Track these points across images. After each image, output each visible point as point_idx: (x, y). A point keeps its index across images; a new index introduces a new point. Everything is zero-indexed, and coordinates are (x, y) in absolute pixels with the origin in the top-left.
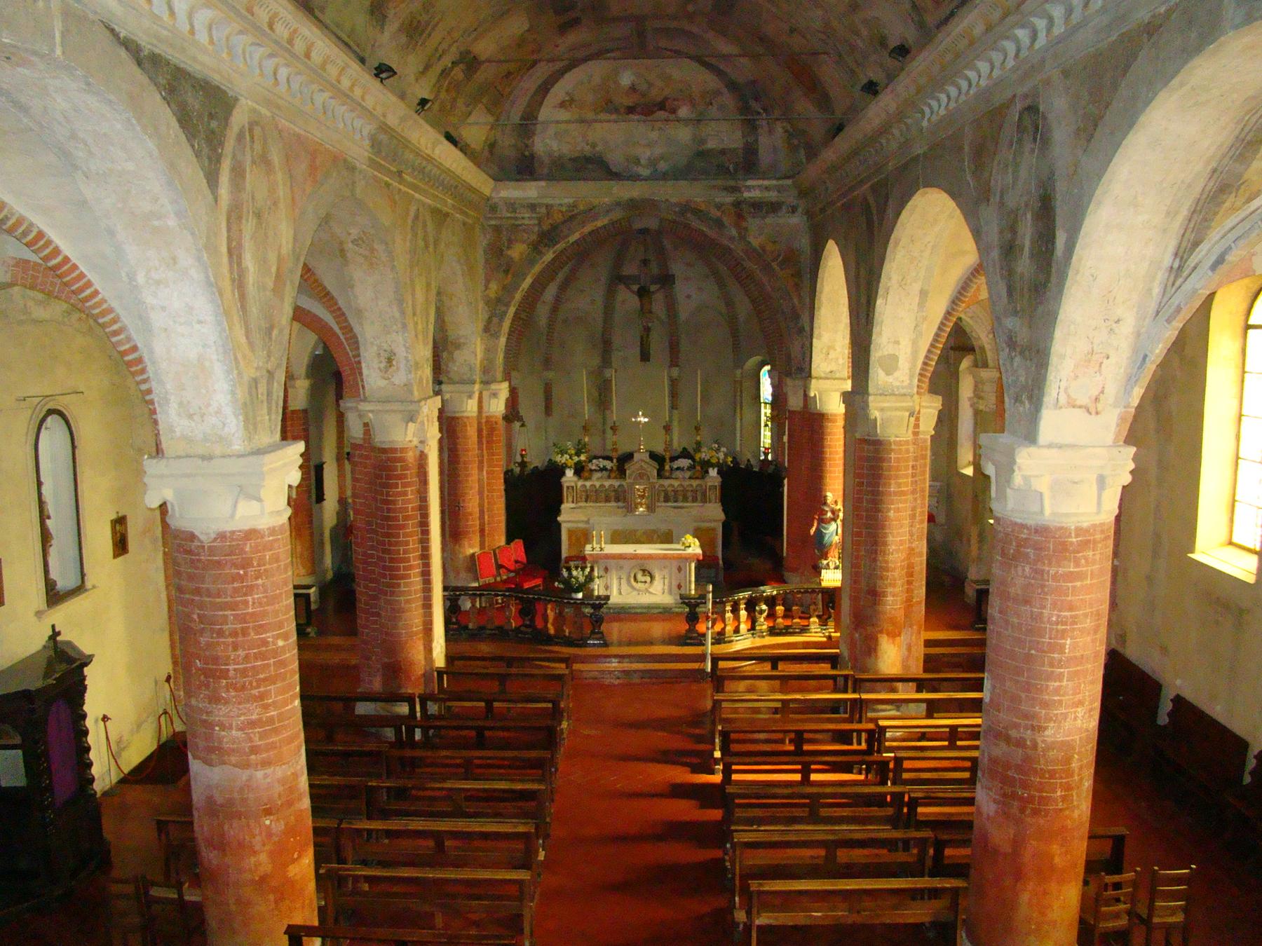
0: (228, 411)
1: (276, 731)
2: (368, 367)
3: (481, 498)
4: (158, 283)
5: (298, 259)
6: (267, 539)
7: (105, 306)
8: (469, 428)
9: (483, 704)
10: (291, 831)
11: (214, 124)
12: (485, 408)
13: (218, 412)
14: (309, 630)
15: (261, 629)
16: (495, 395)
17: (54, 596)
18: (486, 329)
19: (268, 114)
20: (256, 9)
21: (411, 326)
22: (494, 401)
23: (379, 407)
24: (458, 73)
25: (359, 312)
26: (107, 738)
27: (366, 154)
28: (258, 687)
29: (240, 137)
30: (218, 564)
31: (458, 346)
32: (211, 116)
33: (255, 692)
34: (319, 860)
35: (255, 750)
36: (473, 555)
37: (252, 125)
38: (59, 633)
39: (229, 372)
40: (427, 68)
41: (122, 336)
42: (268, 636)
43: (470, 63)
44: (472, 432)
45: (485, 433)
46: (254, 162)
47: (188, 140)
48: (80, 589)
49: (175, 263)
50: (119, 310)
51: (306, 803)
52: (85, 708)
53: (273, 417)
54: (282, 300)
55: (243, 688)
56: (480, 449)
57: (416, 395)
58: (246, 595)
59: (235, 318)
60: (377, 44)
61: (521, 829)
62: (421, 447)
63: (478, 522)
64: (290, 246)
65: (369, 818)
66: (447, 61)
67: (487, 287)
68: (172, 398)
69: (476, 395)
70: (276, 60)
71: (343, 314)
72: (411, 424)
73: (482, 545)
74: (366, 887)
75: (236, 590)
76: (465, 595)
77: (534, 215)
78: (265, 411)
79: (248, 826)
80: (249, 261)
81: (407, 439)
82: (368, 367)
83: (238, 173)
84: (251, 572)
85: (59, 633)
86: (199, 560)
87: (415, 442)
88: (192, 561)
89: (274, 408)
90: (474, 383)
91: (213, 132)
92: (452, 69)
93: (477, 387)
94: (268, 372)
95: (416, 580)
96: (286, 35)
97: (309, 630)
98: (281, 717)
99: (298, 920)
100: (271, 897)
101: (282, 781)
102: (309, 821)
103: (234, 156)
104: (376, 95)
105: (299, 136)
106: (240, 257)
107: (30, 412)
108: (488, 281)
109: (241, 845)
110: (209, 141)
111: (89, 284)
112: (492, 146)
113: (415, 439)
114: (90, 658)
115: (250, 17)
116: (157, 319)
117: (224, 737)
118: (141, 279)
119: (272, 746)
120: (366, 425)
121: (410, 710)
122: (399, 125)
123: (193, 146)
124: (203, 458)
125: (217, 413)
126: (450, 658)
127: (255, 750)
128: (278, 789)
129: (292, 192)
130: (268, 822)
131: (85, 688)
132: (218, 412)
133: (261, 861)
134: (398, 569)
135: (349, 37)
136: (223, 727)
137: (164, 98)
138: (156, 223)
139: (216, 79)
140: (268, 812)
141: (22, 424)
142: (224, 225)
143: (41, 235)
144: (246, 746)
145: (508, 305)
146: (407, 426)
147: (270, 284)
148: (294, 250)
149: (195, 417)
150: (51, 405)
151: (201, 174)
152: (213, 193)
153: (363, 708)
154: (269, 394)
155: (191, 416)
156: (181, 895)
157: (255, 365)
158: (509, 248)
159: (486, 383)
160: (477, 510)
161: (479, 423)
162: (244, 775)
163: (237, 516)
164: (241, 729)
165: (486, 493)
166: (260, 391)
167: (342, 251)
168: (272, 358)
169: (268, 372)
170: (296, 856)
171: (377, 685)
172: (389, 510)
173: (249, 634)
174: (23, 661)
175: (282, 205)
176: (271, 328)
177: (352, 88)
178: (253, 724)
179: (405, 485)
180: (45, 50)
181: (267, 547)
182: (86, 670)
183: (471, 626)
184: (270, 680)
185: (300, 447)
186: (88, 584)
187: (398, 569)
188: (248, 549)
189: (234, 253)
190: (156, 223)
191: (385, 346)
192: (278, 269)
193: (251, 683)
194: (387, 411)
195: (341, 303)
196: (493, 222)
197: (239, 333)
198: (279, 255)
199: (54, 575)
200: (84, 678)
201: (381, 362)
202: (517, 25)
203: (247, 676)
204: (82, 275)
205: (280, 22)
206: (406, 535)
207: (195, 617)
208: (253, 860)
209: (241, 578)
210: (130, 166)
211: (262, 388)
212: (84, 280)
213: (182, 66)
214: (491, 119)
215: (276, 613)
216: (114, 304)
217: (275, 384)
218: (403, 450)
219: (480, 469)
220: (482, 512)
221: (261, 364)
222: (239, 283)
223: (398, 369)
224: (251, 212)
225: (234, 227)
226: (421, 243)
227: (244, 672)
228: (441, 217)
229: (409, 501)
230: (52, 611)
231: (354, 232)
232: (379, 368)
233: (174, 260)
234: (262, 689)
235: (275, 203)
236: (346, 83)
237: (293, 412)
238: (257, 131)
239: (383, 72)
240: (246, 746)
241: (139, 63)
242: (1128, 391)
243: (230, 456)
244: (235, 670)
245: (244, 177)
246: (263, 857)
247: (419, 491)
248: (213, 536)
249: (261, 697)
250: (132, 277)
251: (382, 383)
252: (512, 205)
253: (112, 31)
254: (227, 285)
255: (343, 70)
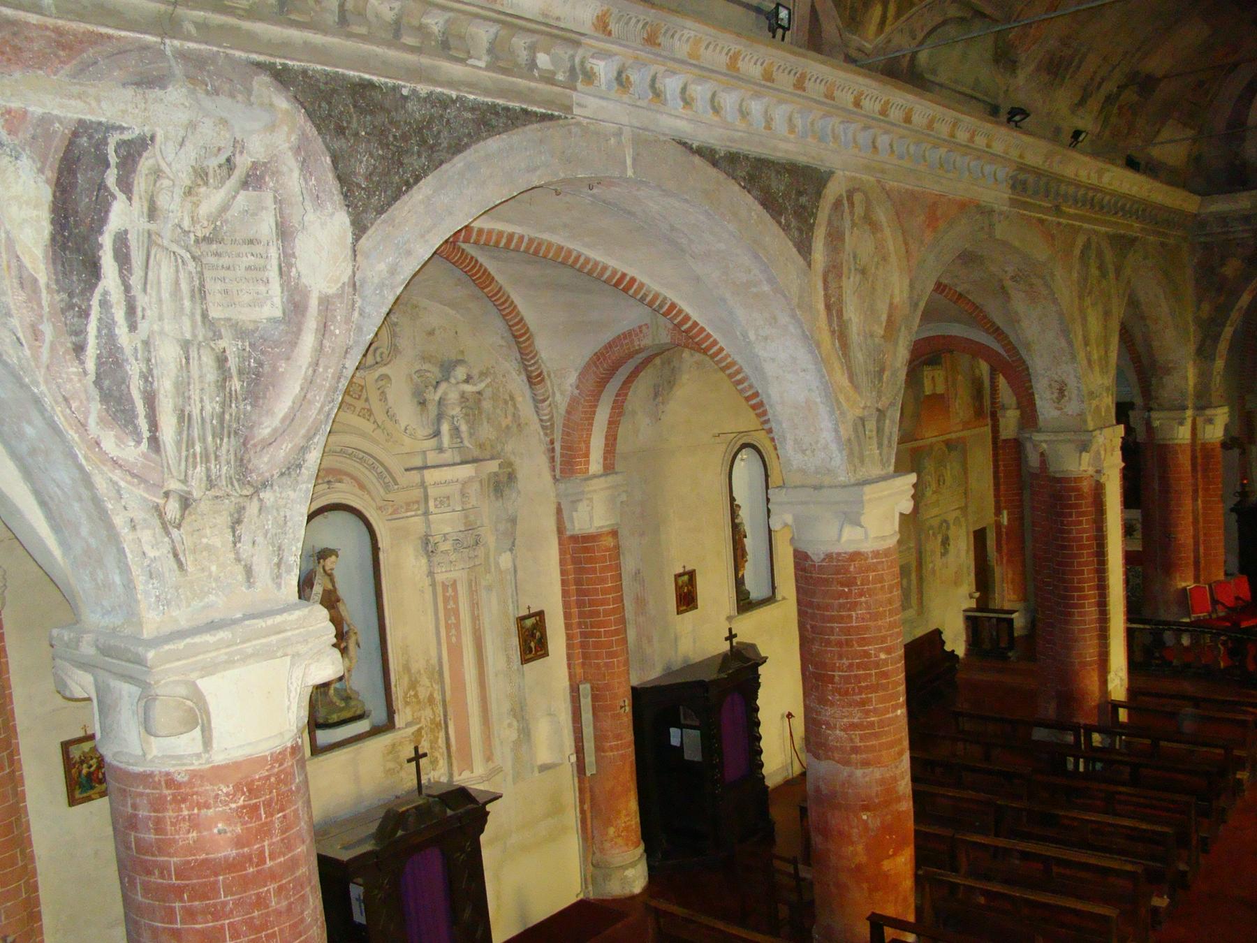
0: (834, 447)
1: (876, 735)
2: (1041, 398)
3: (1196, 530)
4: (766, 338)
5: (916, 305)
6: (870, 561)
7: (729, 360)
8: (1180, 456)
9: (1148, 741)
10: (887, 828)
11: (803, 200)
12: (1200, 435)
13: (825, 447)
14: (1010, 654)
15: (863, 641)
16: (1210, 421)
17: (745, 603)
18: (1200, 351)
19: (872, 179)
20: (837, 93)
21: (1081, 355)
22: (1209, 428)
23: (1052, 437)
24: (1130, 96)
25: (1028, 346)
26: (791, 735)
27: (1006, 196)
28: (860, 693)
29: (837, 204)
30: (826, 582)
31: (1168, 371)
32: (800, 193)
33: (857, 698)
34: (920, 860)
35: (855, 750)
36: (1184, 589)
37: (850, 194)
38: (735, 636)
39: (832, 412)
40: (1082, 102)
41: (746, 384)
42: (871, 649)
43: (1146, 84)
44: (1185, 461)
45: (1199, 461)
46: (854, 225)
47: (774, 218)
48: (770, 600)
49: (776, 322)
50: (740, 361)
51: (907, 806)
52: (758, 702)
53: (885, 450)
54: (896, 343)
55: (847, 693)
56: (1194, 477)
57: (1091, 426)
58: (849, 610)
59: (837, 365)
60: (1011, 89)
61: (1128, 867)
62: (1097, 477)
63: (1192, 555)
64: (905, 295)
65: (997, 835)
66: (1110, 87)
67: (1199, 309)
68: (788, 436)
69: (1189, 422)
70: (872, 131)
71: (1015, 348)
72: (1084, 454)
73: (1197, 579)
74: (982, 900)
75: (841, 606)
76: (1168, 630)
77: (1247, 227)
78: (875, 446)
79: (848, 818)
80: (852, 313)
81: (1082, 468)
82: (1041, 398)
83: (835, 238)
84: (855, 590)
85: (735, 636)
86: (811, 577)
87: (1091, 471)
88: (806, 578)
89: (886, 442)
90: (1184, 408)
91: (803, 207)
92: (1119, 95)
93: (1189, 413)
94: (878, 410)
95: (1091, 611)
96: (878, 107)
97: (1010, 654)
98: (882, 724)
99: (890, 911)
100: (865, 885)
101: (882, 782)
102: (910, 824)
103: (830, 223)
104: (1003, 140)
105: (912, 193)
106: (840, 313)
107: (724, 446)
108: (1200, 302)
109: (841, 833)
110: (797, 214)
111: (715, 343)
112: (1197, 160)
113: (1090, 468)
114: (767, 658)
115: (832, 102)
116: (770, 369)
117: (830, 735)
118: (752, 336)
119: (871, 749)
120: (1042, 454)
121: (1091, 738)
122: (1045, 162)
123: (779, 223)
124: (815, 488)
125: (824, 449)
126: (1132, 691)
127: (855, 750)
128: (876, 789)
129: (906, 244)
130: (865, 817)
131: (758, 685)
132: (825, 447)
133: (857, 852)
134: (1072, 598)
135: (973, 89)
136: (827, 724)
137: (744, 188)
138: (754, 290)
139: (802, 160)
140: (866, 808)
141: (717, 459)
142: (820, 285)
143: (673, 306)
144: (848, 745)
145: (1223, 325)
146: (1080, 457)
147: (881, 331)
148: (911, 298)
149: (807, 452)
150: (745, 440)
151: (790, 244)
152: (805, 259)
153: (1039, 734)
154: (880, 431)
155: (804, 452)
156: (796, 869)
157: (862, 406)
158: (1222, 265)
159: (1200, 408)
160: (1190, 542)
161: (1193, 451)
162: (846, 771)
163: (844, 539)
164: (841, 730)
165: (1201, 524)
166: (867, 428)
167: (1003, 287)
168: (883, 398)
169: (878, 410)
170: (891, 852)
171: (1050, 710)
172: (1063, 539)
173: (852, 646)
174: (709, 659)
175: (893, 259)
176: (882, 371)
177: (971, 140)
178: (853, 726)
179: (1080, 514)
180: (617, 174)
181: (873, 568)
182: (760, 669)
183: (1175, 662)
184: (873, 688)
185: (912, 478)
186: (779, 597)
187: (1072, 598)
188: (852, 569)
189: (834, 308)
190: (754, 290)
191: (1056, 378)
192: (890, 316)
193: (853, 689)
194: (1061, 441)
195: (1012, 338)
196: (1202, 239)
197: (842, 379)
198: (891, 304)
199: (749, 585)
200: (758, 676)
201: (1052, 393)
202: (1193, 34)
203: (851, 683)
204: (709, 336)
205: (868, 98)
206: (1080, 564)
207: (808, 627)
208: (851, 848)
209: (847, 596)
210: (722, 246)
211: (871, 425)
212: (711, 340)
213: (763, 157)
214: (1190, 133)
215: (879, 629)
216: (738, 358)
217: (887, 421)
218: (1076, 479)
219: (1195, 499)
220: (1196, 544)
221: (869, 404)
222: (841, 335)
223: (1070, 399)
224: (853, 269)
225: (833, 285)
226: (1094, 271)
227: (847, 679)
228: (1123, 244)
229: (1084, 531)
230: (740, 617)
231: (1010, 270)
232: (1052, 399)
233: (775, 318)
234: (864, 696)
235: (884, 259)
236: (962, 136)
237: (1005, 441)
238: (858, 197)
239: (1016, 116)
240: (848, 745)
241: (715, 164)
242: (123, 460)
243: (836, 487)
244: (839, 676)
245: (843, 240)
246: (860, 848)
247: (1095, 521)
248: (822, 556)
249: (863, 703)
250: (745, 336)
251: (1056, 413)
252: (1223, 219)
253: (684, 144)
254: (826, 338)
255: (955, 124)
